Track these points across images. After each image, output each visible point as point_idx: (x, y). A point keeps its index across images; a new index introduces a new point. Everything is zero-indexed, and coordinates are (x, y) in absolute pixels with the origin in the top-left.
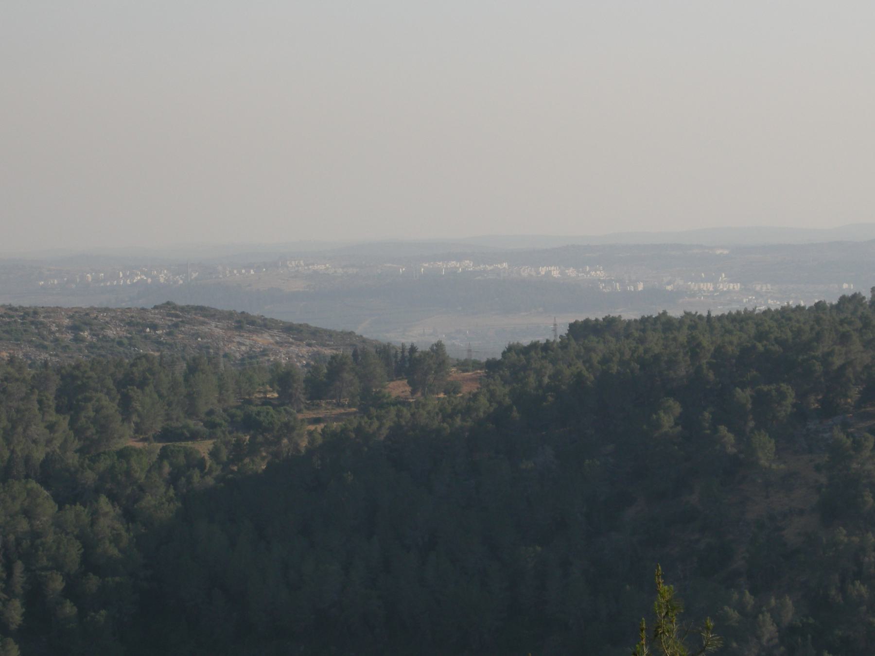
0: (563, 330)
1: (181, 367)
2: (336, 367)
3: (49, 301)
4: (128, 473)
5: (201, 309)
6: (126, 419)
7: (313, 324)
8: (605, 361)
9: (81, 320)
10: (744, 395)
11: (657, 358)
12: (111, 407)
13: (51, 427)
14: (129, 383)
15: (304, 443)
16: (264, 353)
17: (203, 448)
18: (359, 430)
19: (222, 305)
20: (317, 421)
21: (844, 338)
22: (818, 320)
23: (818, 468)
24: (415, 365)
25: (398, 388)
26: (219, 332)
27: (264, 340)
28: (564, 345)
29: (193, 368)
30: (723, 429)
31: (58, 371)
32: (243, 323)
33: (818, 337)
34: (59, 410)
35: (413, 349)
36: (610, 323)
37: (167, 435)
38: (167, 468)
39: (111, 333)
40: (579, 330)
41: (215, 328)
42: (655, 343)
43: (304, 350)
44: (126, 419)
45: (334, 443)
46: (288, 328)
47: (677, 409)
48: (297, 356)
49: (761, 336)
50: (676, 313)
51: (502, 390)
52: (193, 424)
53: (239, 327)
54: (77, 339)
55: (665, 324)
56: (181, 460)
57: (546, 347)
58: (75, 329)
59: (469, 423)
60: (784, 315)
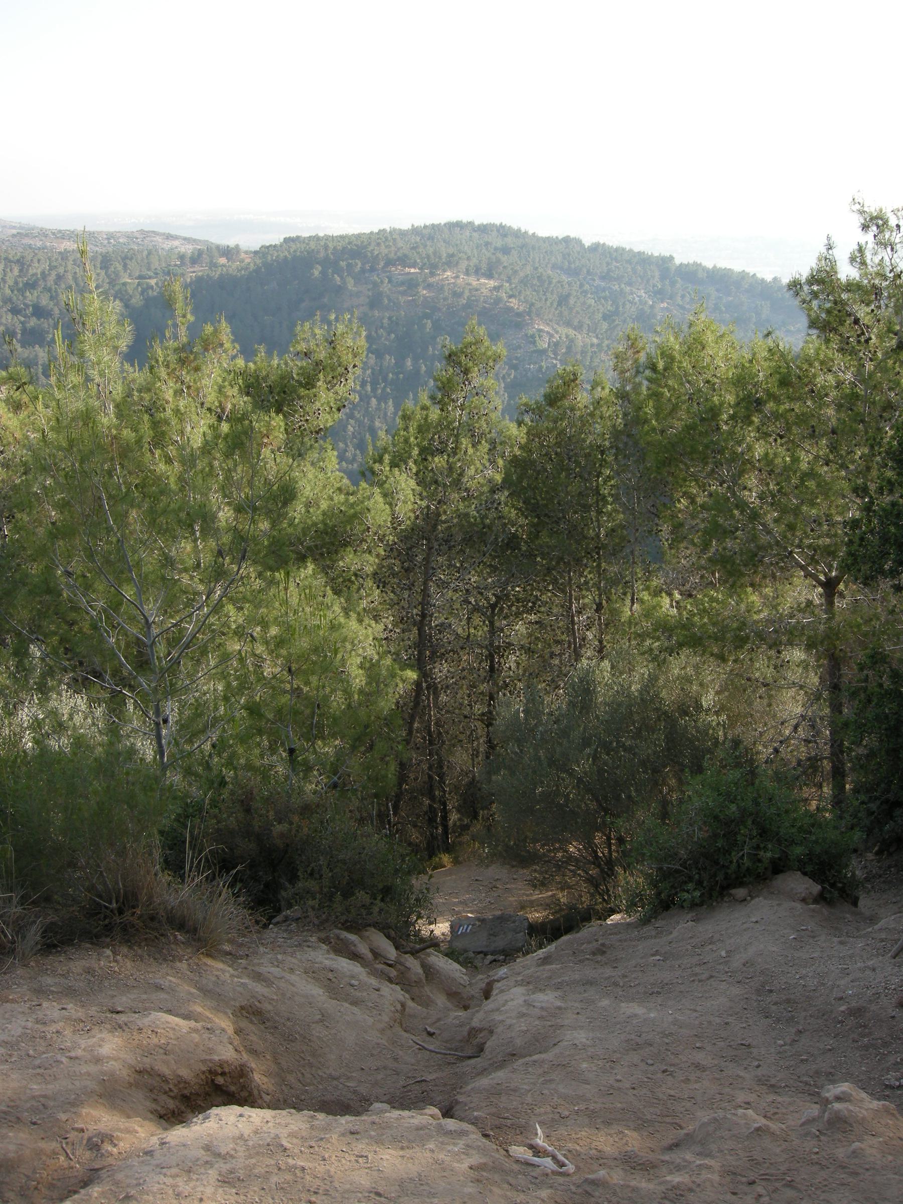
0: (282, 240)
1: (145, 253)
2: (200, 253)
3: (99, 229)
4: (126, 291)
5: (153, 232)
6: (125, 271)
7: (194, 237)
8: (295, 251)
9: (110, 236)
10: (343, 264)
11: (313, 250)
12: (120, 268)
13: (98, 274)
14: (126, 259)
15: (189, 280)
16: (176, 248)
17: (153, 282)
18: (208, 275)
19: (161, 231)
20: (194, 272)
21: (378, 244)
22: (370, 238)
23: (369, 290)
24: (229, 252)
25: (223, 261)
26: (160, 240)
27: (176, 243)
28: (281, 246)
29: (149, 253)
30: (336, 276)
31: (101, 254)
32: (169, 237)
33: (369, 244)
34: (101, 268)
35: (228, 247)
36: (298, 237)
37: (140, 277)
38: (140, 289)
39: (121, 240)
40: (287, 240)
41: (159, 239)
42: (313, 245)
43: (191, 247)
44: (125, 271)
45: (199, 280)
46: (185, 239)
47: (320, 268)
48: (188, 249)
49: (350, 243)
50: (321, 234)
51: (259, 262)
52: (151, 273)
53: (167, 238)
54: (109, 243)
55: (317, 238)
56: (145, 286)
57: (275, 246)
58: (108, 239)
59: (247, 273)
60: (359, 236)
